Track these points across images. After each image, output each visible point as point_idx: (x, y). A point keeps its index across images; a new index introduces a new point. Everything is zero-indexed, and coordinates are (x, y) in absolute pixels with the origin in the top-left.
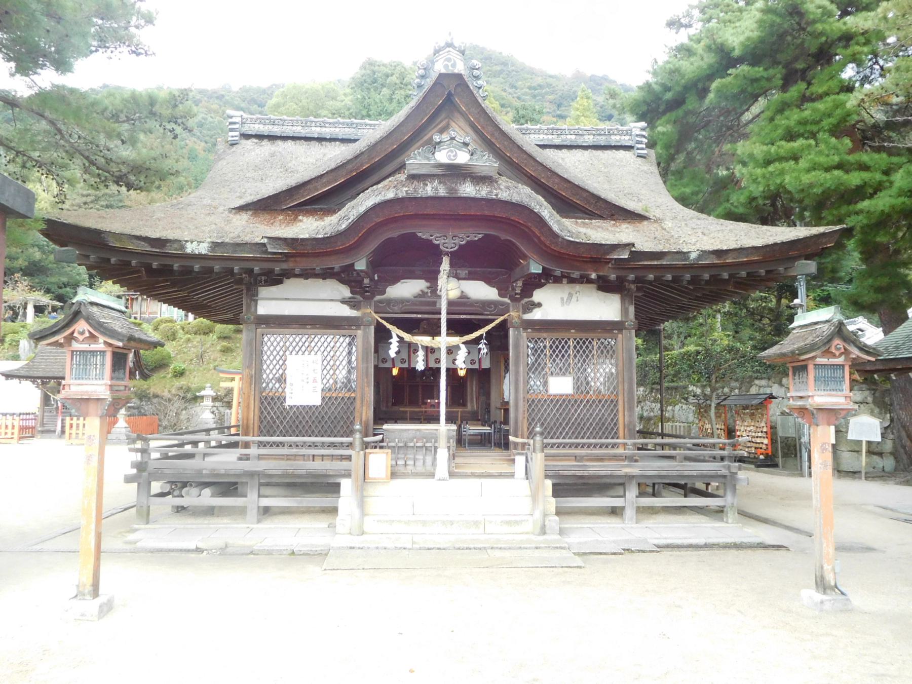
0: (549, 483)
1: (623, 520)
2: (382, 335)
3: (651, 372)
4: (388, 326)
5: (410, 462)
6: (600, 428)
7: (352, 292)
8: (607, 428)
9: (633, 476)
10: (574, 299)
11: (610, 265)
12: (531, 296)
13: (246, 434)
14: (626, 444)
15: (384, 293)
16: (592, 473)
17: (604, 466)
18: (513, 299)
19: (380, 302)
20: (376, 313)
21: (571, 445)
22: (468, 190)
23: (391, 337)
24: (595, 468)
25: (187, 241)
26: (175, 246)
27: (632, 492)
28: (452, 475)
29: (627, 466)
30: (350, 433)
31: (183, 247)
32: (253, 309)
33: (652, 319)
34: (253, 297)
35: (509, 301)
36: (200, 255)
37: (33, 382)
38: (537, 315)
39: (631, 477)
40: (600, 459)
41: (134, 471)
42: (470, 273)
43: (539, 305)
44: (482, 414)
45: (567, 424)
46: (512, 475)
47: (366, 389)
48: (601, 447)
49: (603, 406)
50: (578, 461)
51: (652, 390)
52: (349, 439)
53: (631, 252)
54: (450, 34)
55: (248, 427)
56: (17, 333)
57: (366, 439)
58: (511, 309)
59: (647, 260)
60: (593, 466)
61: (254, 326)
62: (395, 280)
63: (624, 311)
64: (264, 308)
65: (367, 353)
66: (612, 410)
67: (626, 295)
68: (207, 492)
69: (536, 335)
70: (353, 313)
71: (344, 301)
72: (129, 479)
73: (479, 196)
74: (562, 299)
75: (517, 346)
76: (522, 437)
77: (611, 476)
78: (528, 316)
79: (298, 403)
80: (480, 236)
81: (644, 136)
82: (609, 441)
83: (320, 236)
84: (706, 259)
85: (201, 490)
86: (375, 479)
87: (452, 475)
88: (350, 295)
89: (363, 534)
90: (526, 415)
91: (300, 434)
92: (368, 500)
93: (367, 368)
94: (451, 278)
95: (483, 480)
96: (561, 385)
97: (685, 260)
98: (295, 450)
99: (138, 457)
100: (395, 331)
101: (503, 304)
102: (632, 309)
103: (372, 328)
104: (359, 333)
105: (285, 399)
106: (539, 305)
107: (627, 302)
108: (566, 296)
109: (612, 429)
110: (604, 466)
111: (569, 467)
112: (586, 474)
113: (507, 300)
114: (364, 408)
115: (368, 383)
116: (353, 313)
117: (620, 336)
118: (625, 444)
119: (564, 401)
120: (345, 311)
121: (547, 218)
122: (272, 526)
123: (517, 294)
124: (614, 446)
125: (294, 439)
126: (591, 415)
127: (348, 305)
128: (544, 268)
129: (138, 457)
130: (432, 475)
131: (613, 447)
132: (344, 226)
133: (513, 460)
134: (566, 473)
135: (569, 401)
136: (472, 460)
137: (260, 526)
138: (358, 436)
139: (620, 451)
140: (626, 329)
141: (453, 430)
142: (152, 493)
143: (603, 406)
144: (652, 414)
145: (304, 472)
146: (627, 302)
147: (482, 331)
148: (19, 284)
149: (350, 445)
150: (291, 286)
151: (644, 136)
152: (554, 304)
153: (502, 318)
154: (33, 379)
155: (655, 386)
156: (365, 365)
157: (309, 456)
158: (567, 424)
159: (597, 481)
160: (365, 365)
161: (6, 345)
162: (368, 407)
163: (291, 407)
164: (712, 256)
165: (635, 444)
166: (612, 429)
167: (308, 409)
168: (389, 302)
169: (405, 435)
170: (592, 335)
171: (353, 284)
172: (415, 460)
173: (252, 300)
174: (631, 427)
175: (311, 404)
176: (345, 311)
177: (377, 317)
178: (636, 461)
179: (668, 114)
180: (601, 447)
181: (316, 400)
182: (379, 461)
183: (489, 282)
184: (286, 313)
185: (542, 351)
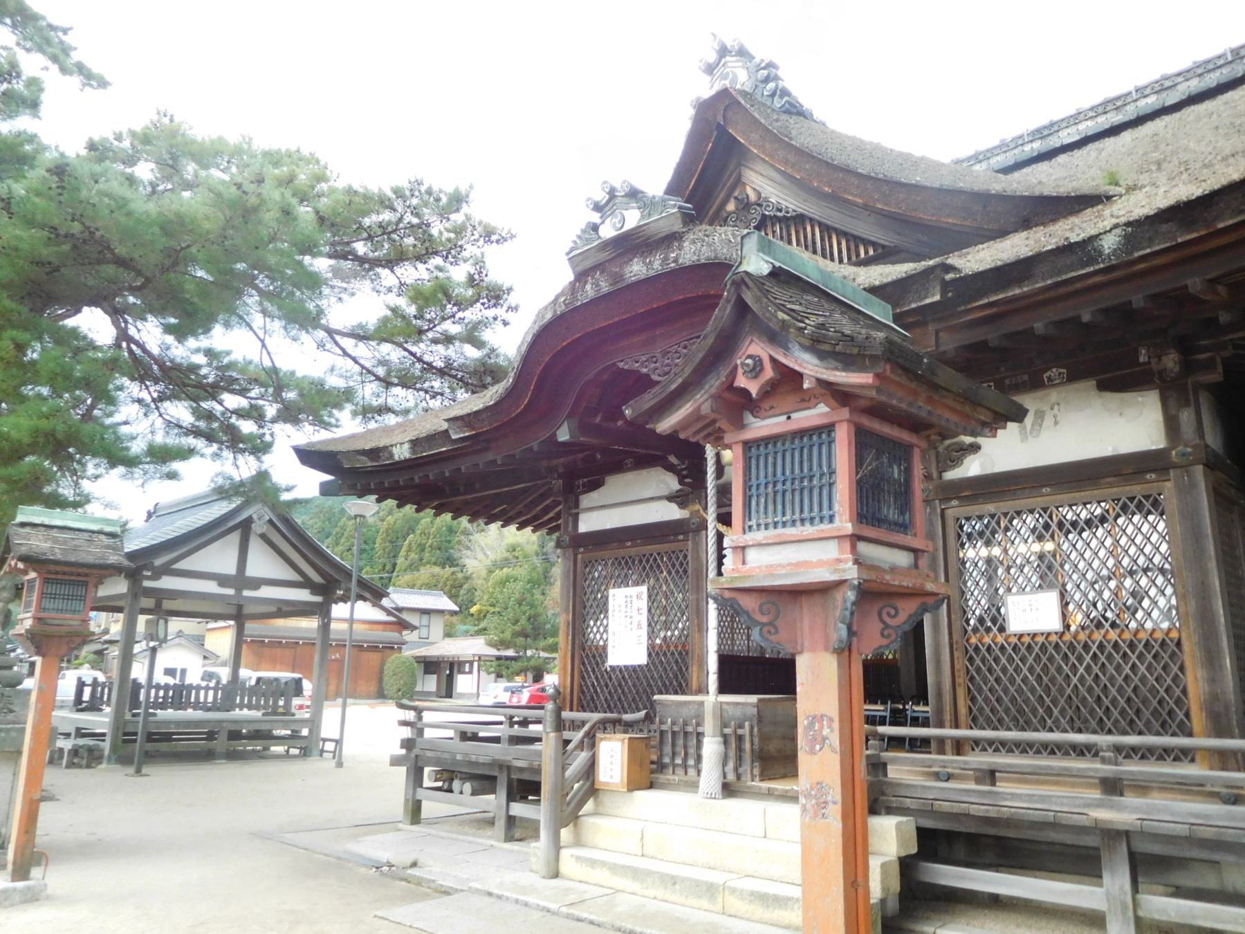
10: (1048, 421)
13: (941, 725)
22: (637, 269)
27: (1117, 879)
31: (391, 455)
36: (406, 461)
41: (403, 752)
54: (715, 36)
61: (571, 550)
71: (670, 498)
72: (396, 761)
73: (652, 273)
76: (957, 726)
78: (952, 475)
84: (1151, 241)
87: (729, 790)
91: (1027, 726)
97: (1092, 260)
99: (407, 733)
112: (993, 812)
124: (1185, 755)
125: (1133, 740)
129: (407, 733)
137: (508, 846)
140: (1175, 466)
150: (618, 486)
159: (1068, 838)
164: (1165, 227)
167: (634, 670)
184: (608, 526)
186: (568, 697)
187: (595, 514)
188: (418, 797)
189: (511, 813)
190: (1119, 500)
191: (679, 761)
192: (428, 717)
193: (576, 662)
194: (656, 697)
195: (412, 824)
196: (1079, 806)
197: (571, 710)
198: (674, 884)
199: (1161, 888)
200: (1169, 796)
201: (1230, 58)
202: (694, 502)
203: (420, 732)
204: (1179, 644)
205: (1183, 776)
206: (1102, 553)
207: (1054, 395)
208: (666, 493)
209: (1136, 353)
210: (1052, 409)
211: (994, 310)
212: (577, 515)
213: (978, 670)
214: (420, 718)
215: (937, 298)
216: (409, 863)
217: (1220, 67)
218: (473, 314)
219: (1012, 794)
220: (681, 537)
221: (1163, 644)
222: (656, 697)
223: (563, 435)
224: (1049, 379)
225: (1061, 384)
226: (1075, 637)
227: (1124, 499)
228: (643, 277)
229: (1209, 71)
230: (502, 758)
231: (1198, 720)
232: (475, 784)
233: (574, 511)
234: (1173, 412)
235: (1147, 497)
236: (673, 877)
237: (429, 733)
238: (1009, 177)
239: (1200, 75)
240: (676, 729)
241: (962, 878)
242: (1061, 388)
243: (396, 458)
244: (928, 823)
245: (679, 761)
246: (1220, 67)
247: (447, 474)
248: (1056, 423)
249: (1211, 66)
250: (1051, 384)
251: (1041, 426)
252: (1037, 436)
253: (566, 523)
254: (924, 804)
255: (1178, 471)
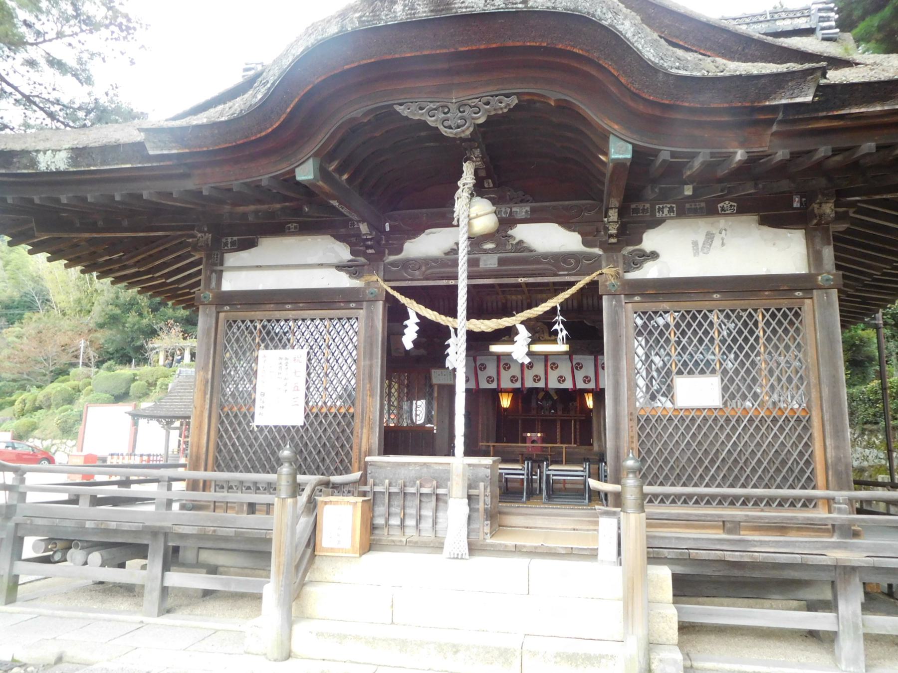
0: (663, 575)
1: (837, 661)
2: (396, 315)
3: (861, 408)
4: (403, 299)
5: (410, 522)
6: (778, 471)
7: (352, 253)
8: (791, 470)
9: (854, 569)
10: (717, 242)
11: (775, 128)
12: (640, 241)
14: (836, 502)
15: (400, 250)
16: (759, 557)
17: (787, 544)
18: (608, 248)
19: (393, 264)
20: (385, 281)
21: (722, 500)
23: (407, 317)
24: (766, 548)
25: (38, 151)
26: (25, 161)
27: (851, 604)
28: (473, 548)
29: (836, 546)
30: (810, 483)
31: (34, 163)
32: (213, 284)
33: (865, 301)
34: (217, 267)
35: (601, 252)
36: (58, 173)
37: (160, 422)
38: (650, 271)
39: (849, 570)
40: (782, 528)
42: (533, 210)
43: (654, 255)
44: (544, 437)
45: (713, 462)
46: (592, 554)
47: (368, 399)
48: (780, 505)
49: (782, 429)
50: (730, 532)
51: (863, 433)
52: (272, 477)
53: (820, 88)
55: (198, 458)
56: (166, 377)
57: (647, 489)
58: (604, 264)
59: (858, 104)
60: (762, 543)
61: (213, 308)
62: (416, 231)
63: (815, 257)
64: (231, 282)
65: (371, 345)
66: (800, 438)
67: (815, 230)
68: (96, 557)
69: (650, 307)
70: (356, 283)
71: (340, 267)
74: (695, 244)
75: (615, 325)
77: (803, 566)
79: (271, 423)
80: (514, 101)
81: (831, 10)
82: (797, 492)
83: (223, 119)
85: (89, 554)
86: (332, 550)
87: (473, 548)
88: (350, 257)
89: (289, 656)
90: (636, 445)
92: (310, 590)
93: (371, 367)
94: (477, 200)
95: (538, 563)
96: (699, 392)
98: (225, 494)
100: (414, 308)
101: (588, 257)
102: (828, 253)
103: (380, 305)
104: (362, 313)
105: (253, 417)
106: (654, 255)
107: (818, 240)
108: (701, 239)
109: (802, 471)
110: (787, 544)
111: (707, 539)
112: (746, 558)
113: (597, 251)
114: (365, 431)
115: (372, 390)
116: (356, 283)
117: (808, 301)
118: (830, 501)
119: (705, 419)
120: (343, 281)
121: (629, 35)
122: (178, 622)
123: (611, 236)
124: (807, 503)
126: (759, 445)
127: (348, 272)
128: (636, 151)
130: (437, 546)
131: (804, 505)
132: (259, 96)
133: (597, 523)
134: (703, 555)
135: (716, 420)
136: (539, 522)
137: (166, 620)
138: (285, 469)
139: (820, 514)
140: (820, 288)
141: (486, 467)
142: (24, 557)
143: (782, 429)
144: (865, 464)
145: (230, 532)
146: (818, 240)
147: (555, 302)
148: (173, 331)
149: (271, 488)
150: (271, 249)
151: (831, 10)
152: (678, 251)
153: (587, 279)
154: (158, 418)
155: (868, 426)
156: (368, 362)
157: (242, 504)
158: (713, 462)
160: (368, 362)
161: (158, 388)
162: (371, 429)
163: (261, 429)
165: (850, 501)
166: (802, 471)
168: (407, 264)
169: (403, 472)
170: (755, 303)
171: (354, 239)
172: (419, 519)
173: (213, 271)
174: (841, 468)
175: (289, 423)
176: (343, 281)
177: (386, 286)
178: (856, 534)
179: (868, 19)
180: (744, 503)
181: (297, 419)
182: (341, 518)
183: (567, 223)
184: (261, 287)
185: (661, 334)
186: (203, 457)
187: (244, 274)
188: (15, 572)
189: (166, 584)
190: (746, 310)
191: (395, 521)
192: (31, 479)
193: (214, 421)
194: (368, 459)
195: (7, 603)
196: (818, 549)
197: (206, 470)
198: (456, 652)
199: (795, 603)
200: (804, 533)
201: (769, 18)
202: (370, 273)
203: (23, 496)
204: (353, 416)
205: (808, 519)
206: (349, 361)
207: (722, 222)
208: (335, 261)
209: (792, 201)
210: (720, 233)
211: (841, 123)
212: (222, 271)
213: (226, 431)
214: (23, 481)
215: (809, 99)
216: (52, 659)
217: (761, 22)
218: (94, 41)
219: (761, 541)
220: (353, 305)
221: (317, 416)
222: (368, 459)
223: (306, 173)
224: (723, 209)
225: (732, 214)
226: (329, 410)
227: (705, 311)
228: (478, 11)
229: (754, 23)
230: (158, 524)
231: (820, 479)
232: (104, 552)
233: (219, 268)
234: (818, 248)
235: (790, 309)
236: (454, 646)
237: (32, 497)
238: (671, 48)
239: (748, 24)
240: (393, 490)
241: (710, 615)
242: (729, 218)
243: (42, 167)
244: (680, 570)
245: (395, 521)
246: (761, 22)
247: (118, 198)
248: (723, 244)
249: (755, 20)
250: (723, 213)
251: (710, 245)
252: (707, 253)
253: (209, 279)
254: (681, 554)
255: (820, 292)
